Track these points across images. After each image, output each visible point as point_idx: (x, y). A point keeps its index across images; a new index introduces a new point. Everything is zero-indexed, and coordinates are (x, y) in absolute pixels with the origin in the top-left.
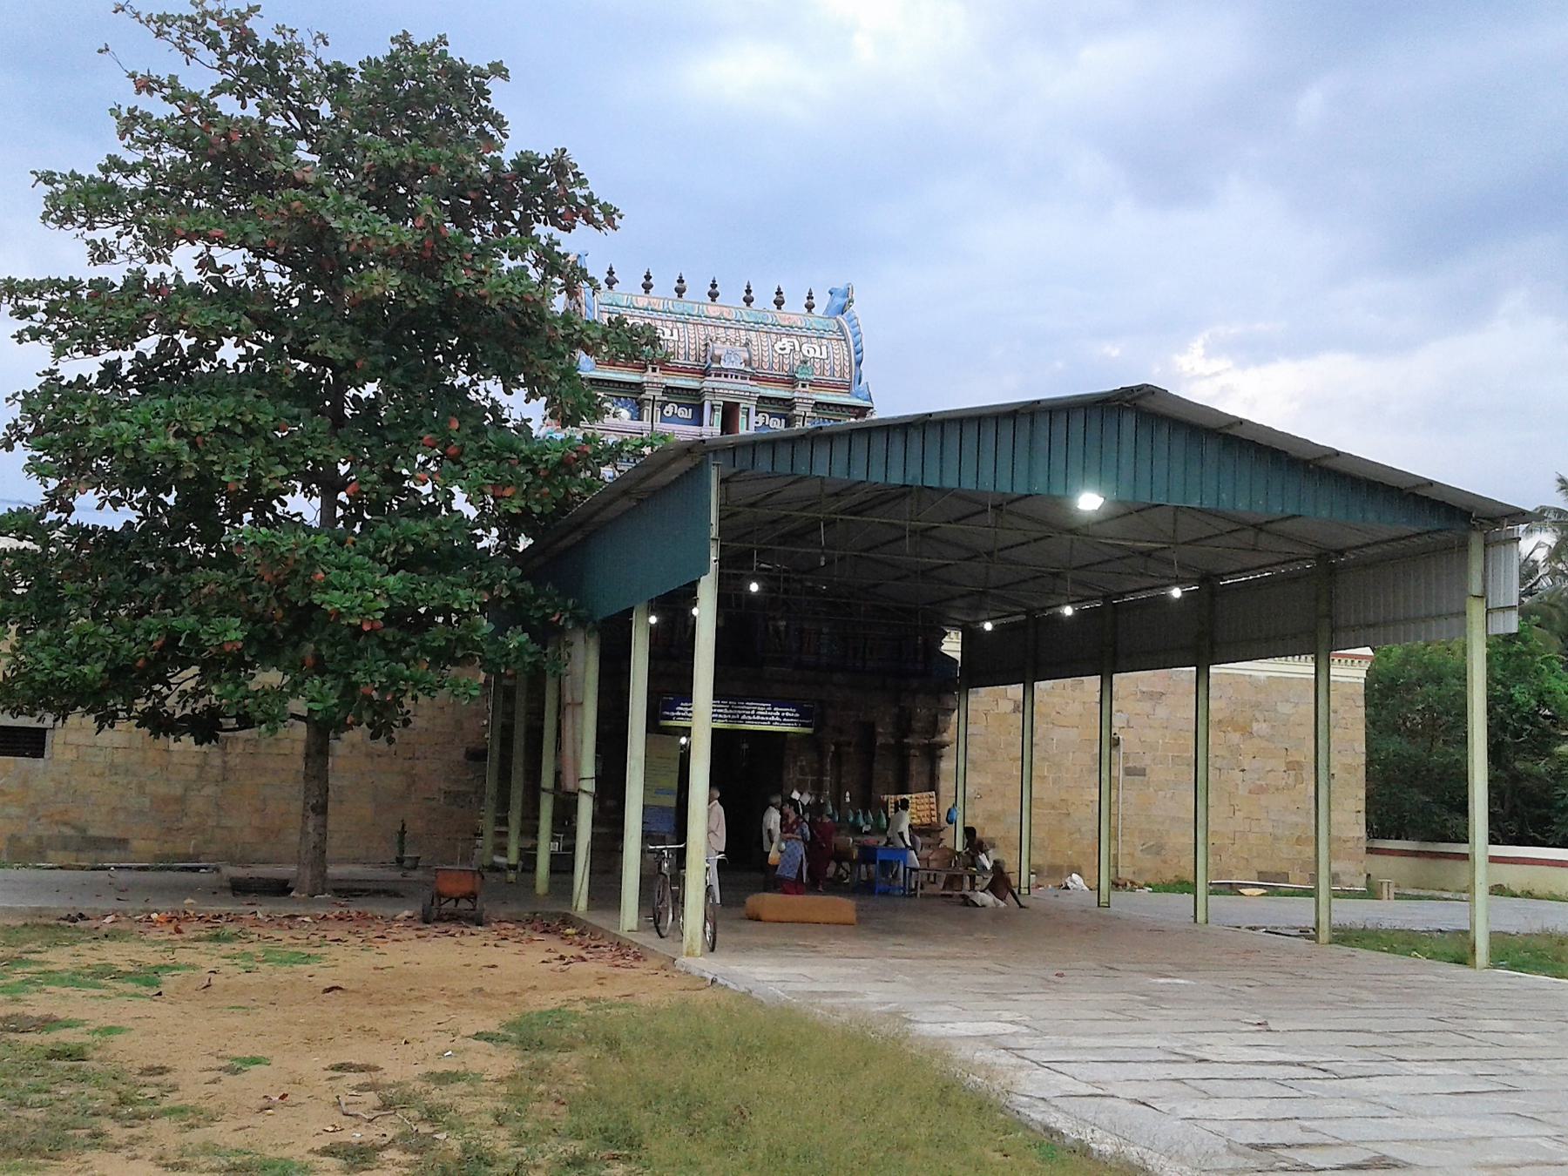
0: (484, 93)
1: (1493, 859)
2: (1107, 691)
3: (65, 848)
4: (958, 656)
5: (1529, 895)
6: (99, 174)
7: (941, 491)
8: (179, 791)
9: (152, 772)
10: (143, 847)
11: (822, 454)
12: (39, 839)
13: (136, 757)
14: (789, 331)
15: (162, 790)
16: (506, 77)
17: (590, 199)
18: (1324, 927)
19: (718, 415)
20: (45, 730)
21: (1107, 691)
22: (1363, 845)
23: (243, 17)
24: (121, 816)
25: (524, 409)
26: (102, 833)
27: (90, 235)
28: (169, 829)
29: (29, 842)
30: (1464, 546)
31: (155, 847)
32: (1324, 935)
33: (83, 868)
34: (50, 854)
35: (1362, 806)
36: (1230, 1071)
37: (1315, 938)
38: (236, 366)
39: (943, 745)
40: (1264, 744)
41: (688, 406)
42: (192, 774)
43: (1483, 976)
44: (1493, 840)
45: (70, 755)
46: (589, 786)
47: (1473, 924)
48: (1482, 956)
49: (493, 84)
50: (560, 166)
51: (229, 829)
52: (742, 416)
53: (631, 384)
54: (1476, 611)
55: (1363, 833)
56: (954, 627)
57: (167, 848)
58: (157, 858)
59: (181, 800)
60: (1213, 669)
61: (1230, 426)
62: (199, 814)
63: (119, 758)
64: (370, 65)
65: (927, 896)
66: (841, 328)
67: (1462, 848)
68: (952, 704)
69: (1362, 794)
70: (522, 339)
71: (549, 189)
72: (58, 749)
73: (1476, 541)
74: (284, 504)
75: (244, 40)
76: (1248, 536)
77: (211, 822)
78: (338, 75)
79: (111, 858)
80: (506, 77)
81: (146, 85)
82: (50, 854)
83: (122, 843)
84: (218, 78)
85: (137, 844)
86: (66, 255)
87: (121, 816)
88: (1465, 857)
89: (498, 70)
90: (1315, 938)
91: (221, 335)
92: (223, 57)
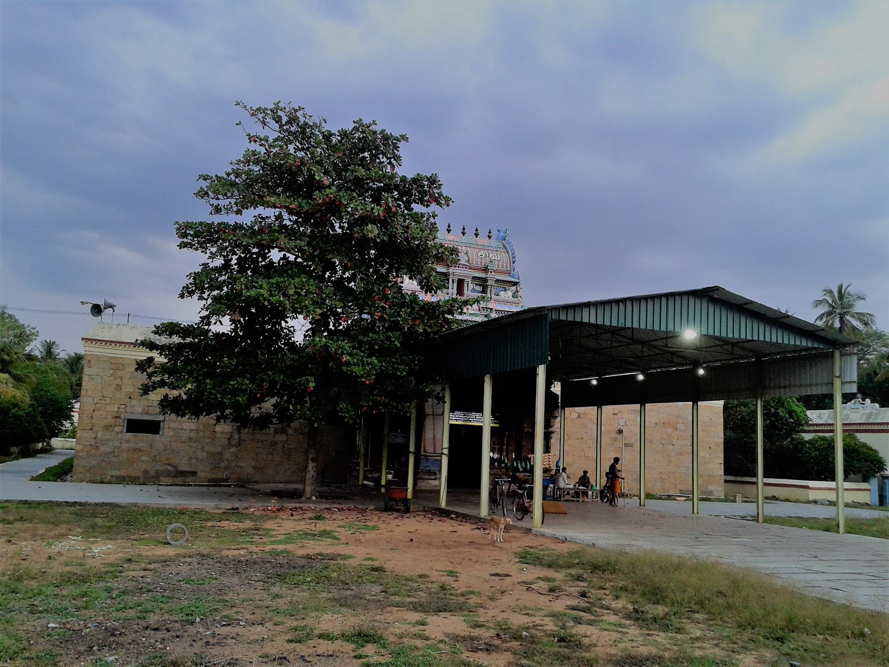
0: (396, 148)
1: (765, 484)
2: (642, 413)
3: (169, 476)
4: (559, 393)
5: (787, 500)
6: (225, 176)
7: (589, 324)
8: (219, 449)
9: (207, 440)
10: (204, 474)
11: (585, 312)
12: (157, 472)
13: (201, 434)
14: (483, 248)
15: (212, 450)
16: (407, 141)
17: (440, 194)
18: (761, 516)
19: (455, 284)
20: (160, 422)
21: (642, 413)
22: (723, 478)
23: (296, 111)
24: (194, 461)
25: (409, 285)
26: (185, 469)
27: (215, 202)
28: (215, 468)
29: (152, 473)
30: (832, 355)
31: (209, 476)
32: (761, 520)
33: (177, 485)
34: (162, 478)
35: (722, 462)
36: (861, 577)
37: (757, 521)
38: (279, 262)
39: (552, 432)
40: (681, 433)
41: (480, 285)
42: (226, 442)
43: (842, 536)
44: (766, 475)
45: (171, 433)
46: (446, 451)
47: (838, 515)
48: (842, 529)
49: (402, 144)
50: (433, 181)
51: (242, 467)
52: (465, 285)
53: (479, 278)
54: (837, 383)
55: (722, 473)
56: (558, 380)
57: (214, 476)
58: (209, 481)
59: (220, 454)
60: (699, 403)
61: (746, 304)
62: (228, 461)
63: (193, 435)
64: (344, 134)
65: (567, 501)
66: (504, 247)
67: (754, 480)
68: (557, 414)
69: (722, 456)
70: (414, 255)
71: (423, 189)
72: (166, 430)
73: (837, 354)
74: (287, 322)
75: (292, 120)
76: (729, 347)
77: (234, 464)
78: (328, 137)
79: (190, 480)
80: (407, 141)
81: (252, 139)
82: (162, 478)
83: (194, 473)
84: (277, 134)
85: (201, 474)
86: (202, 213)
87: (194, 461)
88: (754, 483)
89: (404, 138)
90: (757, 521)
91: (270, 247)
92: (281, 126)
